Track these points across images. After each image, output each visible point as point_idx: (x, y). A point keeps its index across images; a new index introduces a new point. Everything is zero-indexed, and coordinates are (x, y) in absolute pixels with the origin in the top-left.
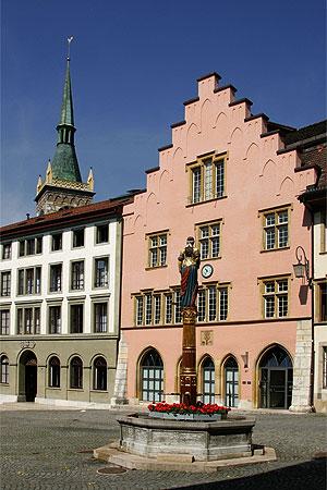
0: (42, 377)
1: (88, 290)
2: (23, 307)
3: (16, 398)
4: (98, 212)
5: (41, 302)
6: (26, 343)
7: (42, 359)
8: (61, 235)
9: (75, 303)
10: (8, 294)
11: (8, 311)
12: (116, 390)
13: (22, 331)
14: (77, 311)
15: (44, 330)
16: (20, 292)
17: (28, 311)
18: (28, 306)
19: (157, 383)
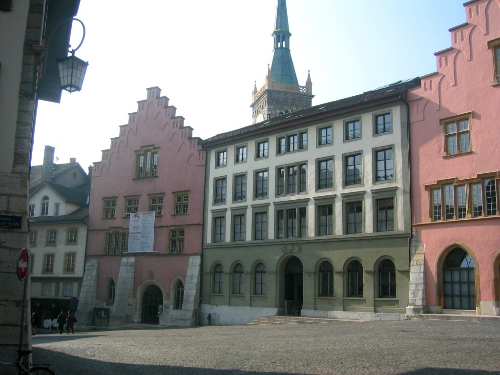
0: (309, 286)
1: (250, 201)
2: (284, 208)
3: (276, 310)
4: (380, 99)
5: (246, 207)
6: (289, 248)
7: (309, 265)
8: (121, 134)
9: (325, 203)
10: (302, 188)
11: (244, 215)
12: (411, 296)
13: (282, 235)
14: (353, 206)
15: (311, 232)
16: (279, 193)
17: (291, 213)
18: (291, 207)
19: (457, 292)
